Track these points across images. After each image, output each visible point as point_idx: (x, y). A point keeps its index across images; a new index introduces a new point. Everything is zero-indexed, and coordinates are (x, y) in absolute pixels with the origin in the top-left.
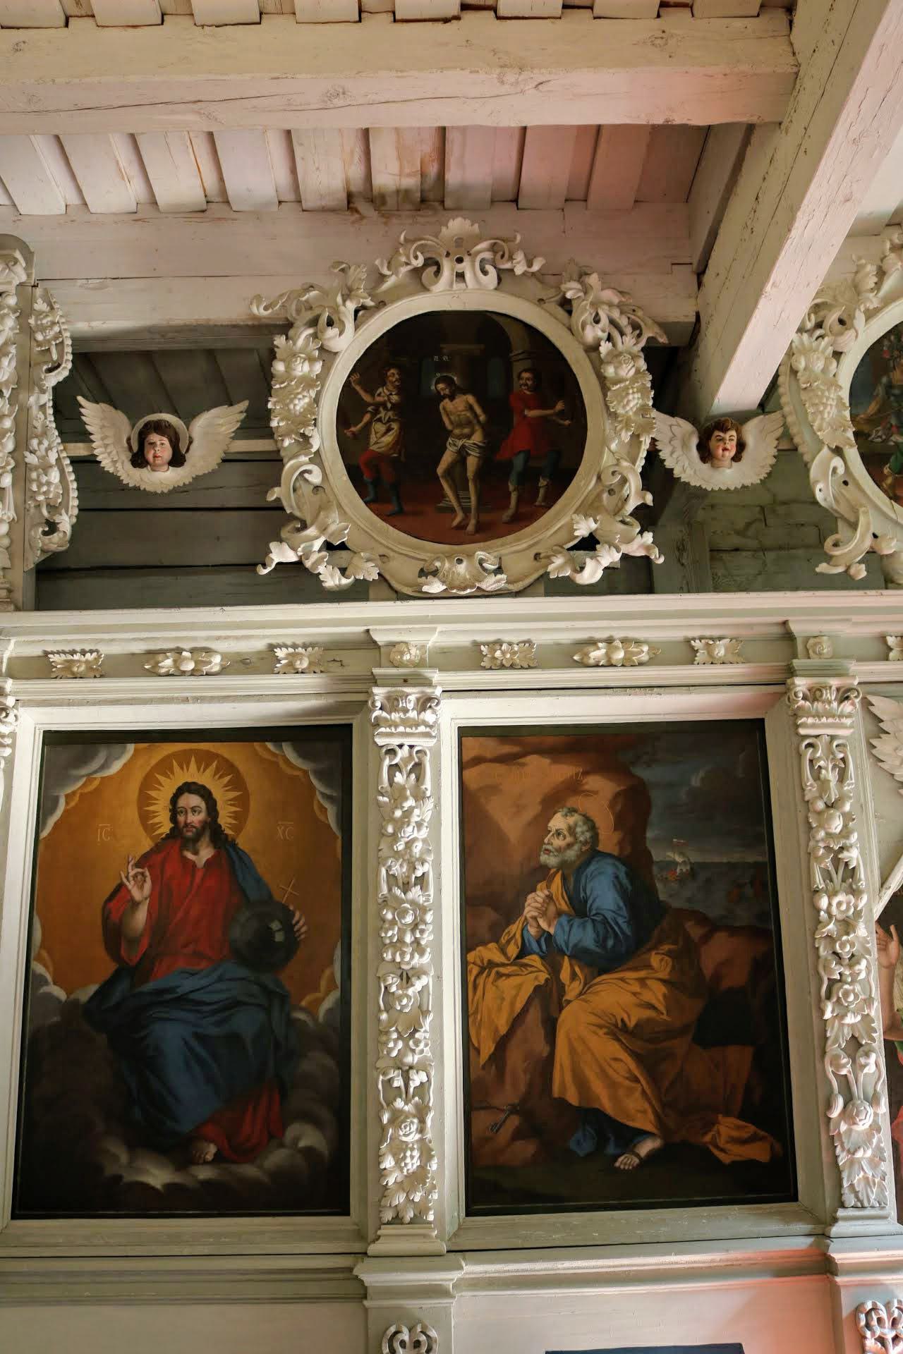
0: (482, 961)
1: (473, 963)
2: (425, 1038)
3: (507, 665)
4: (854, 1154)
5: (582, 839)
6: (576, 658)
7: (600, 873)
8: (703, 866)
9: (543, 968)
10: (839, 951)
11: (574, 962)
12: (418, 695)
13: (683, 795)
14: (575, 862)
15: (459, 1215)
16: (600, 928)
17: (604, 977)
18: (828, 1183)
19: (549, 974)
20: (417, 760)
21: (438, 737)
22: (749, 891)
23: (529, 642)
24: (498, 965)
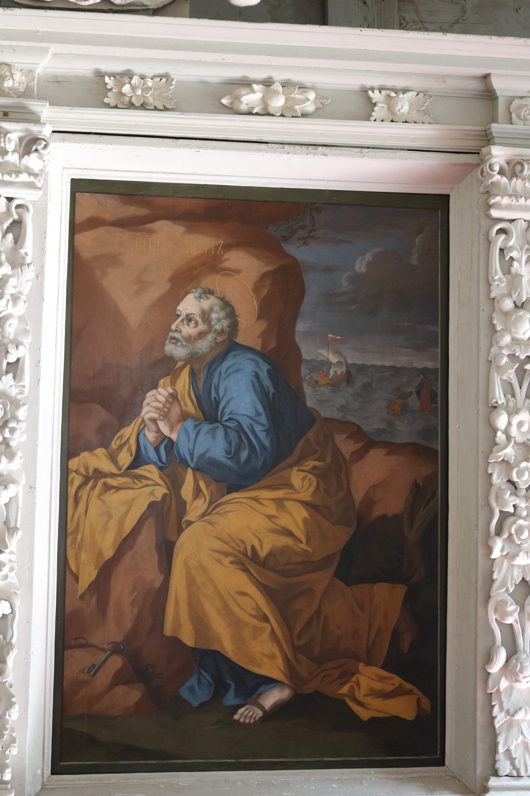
0: (87, 469)
1: (76, 472)
2: (10, 561)
3: (138, 104)
4: (513, 715)
5: (218, 327)
6: (225, 101)
7: (237, 371)
8: (362, 368)
9: (160, 482)
10: (515, 478)
11: (198, 474)
12: (21, 134)
13: (344, 283)
14: (207, 355)
15: (43, 773)
16: (233, 435)
17: (234, 495)
18: (481, 747)
19: (168, 489)
20: (16, 217)
21: (44, 189)
22: (414, 402)
23: (166, 76)
24: (106, 475)
